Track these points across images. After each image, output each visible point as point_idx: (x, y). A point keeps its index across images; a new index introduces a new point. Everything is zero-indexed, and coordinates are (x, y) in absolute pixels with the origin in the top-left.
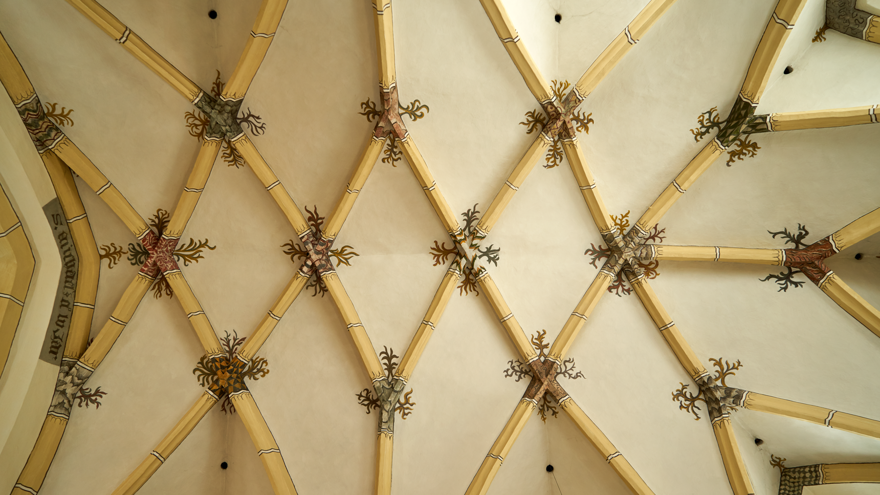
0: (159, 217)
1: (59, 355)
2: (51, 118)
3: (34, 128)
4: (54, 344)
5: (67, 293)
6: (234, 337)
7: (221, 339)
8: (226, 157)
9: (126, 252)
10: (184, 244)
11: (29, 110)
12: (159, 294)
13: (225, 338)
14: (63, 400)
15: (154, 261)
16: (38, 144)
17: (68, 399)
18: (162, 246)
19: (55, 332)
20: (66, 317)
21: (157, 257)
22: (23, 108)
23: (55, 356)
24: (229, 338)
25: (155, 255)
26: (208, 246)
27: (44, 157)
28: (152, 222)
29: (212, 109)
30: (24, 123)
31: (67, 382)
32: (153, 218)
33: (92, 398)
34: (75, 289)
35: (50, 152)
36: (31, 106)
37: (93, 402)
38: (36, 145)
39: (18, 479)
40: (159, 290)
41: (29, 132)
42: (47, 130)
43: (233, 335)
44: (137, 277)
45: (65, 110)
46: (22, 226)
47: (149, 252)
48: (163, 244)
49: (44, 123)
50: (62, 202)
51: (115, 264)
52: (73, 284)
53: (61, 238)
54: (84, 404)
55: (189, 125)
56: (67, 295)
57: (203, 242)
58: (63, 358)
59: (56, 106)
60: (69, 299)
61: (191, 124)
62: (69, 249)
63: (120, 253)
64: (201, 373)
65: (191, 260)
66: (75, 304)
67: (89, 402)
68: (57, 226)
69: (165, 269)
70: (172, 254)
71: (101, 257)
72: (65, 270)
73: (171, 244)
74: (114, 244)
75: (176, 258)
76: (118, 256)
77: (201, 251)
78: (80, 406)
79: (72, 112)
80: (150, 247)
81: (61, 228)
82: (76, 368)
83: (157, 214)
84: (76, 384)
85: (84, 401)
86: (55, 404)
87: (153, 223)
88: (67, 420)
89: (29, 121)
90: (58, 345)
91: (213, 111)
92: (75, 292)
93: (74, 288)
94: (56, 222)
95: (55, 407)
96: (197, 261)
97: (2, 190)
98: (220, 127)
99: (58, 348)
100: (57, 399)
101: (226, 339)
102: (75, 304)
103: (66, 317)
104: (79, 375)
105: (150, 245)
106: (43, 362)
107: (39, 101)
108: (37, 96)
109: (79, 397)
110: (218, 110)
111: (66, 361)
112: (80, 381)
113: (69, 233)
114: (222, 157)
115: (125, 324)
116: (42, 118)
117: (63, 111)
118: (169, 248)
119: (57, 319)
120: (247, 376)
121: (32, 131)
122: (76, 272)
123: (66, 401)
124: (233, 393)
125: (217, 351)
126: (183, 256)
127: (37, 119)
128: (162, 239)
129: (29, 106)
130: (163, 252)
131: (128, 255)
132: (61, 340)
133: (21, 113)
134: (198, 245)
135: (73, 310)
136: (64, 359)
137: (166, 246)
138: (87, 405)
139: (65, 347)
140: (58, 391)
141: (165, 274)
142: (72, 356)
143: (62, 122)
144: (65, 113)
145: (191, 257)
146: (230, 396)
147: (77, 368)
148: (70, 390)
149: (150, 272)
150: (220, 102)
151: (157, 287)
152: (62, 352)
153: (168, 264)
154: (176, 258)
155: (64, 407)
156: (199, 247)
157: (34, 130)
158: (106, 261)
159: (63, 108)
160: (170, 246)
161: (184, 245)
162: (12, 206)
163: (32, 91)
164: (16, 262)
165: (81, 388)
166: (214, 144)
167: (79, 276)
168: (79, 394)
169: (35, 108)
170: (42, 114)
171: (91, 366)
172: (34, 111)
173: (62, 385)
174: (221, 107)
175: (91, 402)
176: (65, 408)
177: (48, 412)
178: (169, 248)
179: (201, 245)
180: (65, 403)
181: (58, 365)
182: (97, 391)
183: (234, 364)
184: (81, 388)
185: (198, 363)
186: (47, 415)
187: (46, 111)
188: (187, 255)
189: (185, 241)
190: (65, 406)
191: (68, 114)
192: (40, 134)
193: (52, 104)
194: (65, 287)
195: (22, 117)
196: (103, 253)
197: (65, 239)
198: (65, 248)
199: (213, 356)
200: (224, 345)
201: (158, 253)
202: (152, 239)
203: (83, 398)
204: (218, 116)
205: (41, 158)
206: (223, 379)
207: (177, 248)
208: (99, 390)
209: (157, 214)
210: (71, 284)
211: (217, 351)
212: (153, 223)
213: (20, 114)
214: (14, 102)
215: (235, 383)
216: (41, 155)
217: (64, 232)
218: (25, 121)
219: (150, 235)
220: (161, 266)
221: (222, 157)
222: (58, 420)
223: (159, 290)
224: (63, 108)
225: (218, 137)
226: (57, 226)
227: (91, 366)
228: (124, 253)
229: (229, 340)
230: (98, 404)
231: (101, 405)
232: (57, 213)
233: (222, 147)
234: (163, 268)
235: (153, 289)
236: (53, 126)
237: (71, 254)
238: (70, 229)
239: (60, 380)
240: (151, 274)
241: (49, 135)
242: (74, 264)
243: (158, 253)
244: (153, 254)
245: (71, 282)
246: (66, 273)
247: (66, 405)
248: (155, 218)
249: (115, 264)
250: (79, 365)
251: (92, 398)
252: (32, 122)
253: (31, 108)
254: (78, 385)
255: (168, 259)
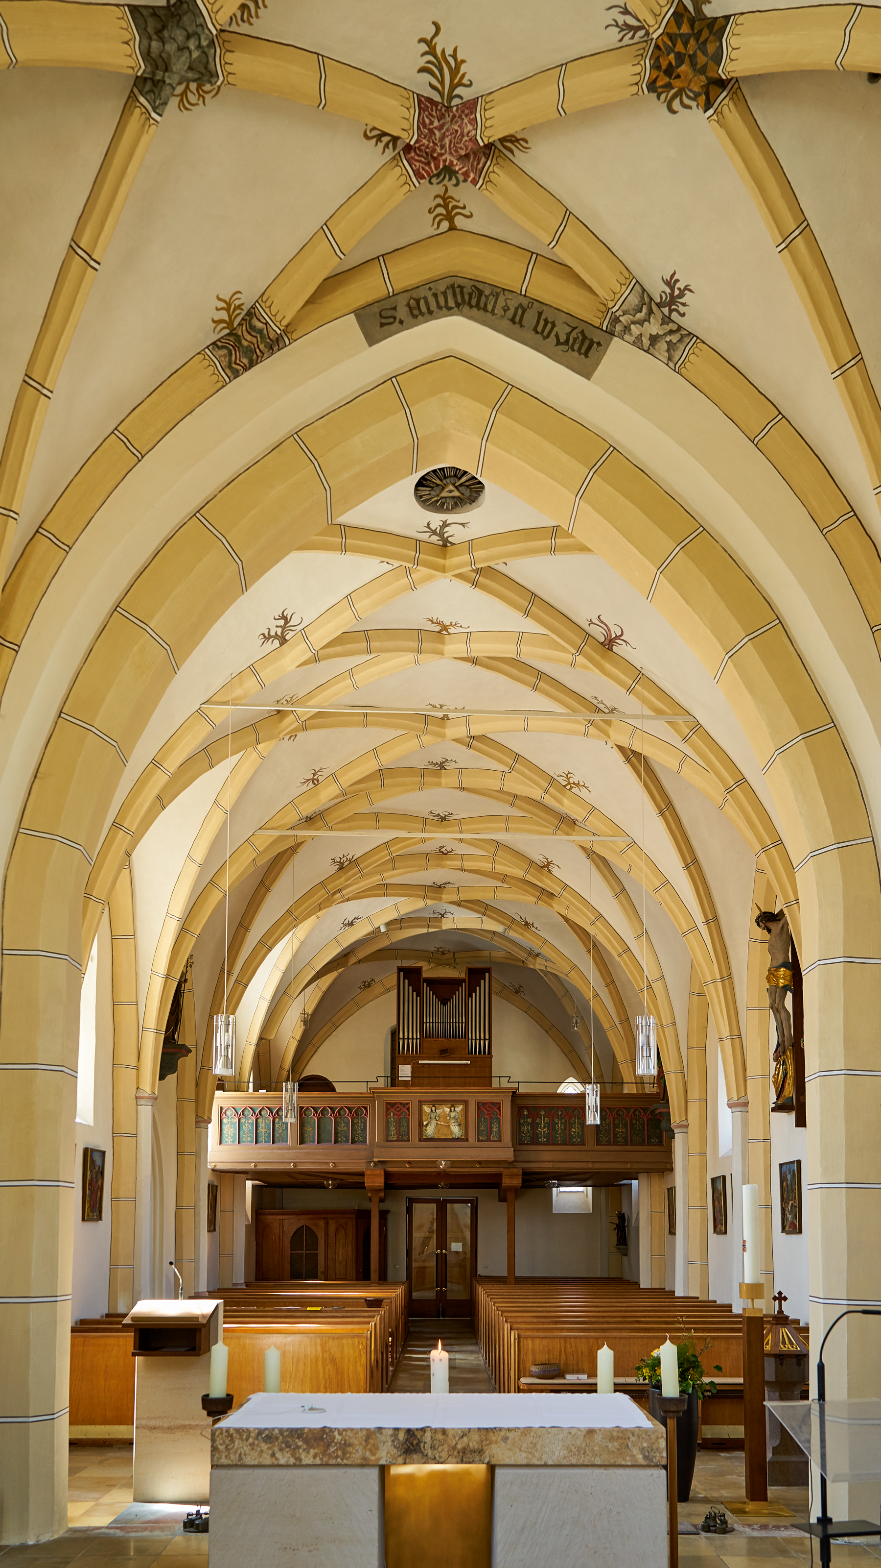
0: (379, 135)
1: (596, 336)
2: (236, 323)
3: (255, 356)
4: (576, 347)
5: (503, 308)
6: (621, 12)
7: (621, 40)
8: (250, 15)
9: (444, 188)
10: (430, 84)
11: (230, 362)
12: (521, 142)
13: (619, 32)
14: (666, 342)
15: (458, 160)
16: (277, 347)
17: (665, 335)
18: (431, 144)
19: (558, 343)
20: (540, 314)
21: (451, 153)
22: (227, 371)
23: (595, 345)
24: (621, 23)
25: (448, 157)
26: (433, 38)
27: (294, 336)
28: (388, 148)
29: (164, 82)
30: (250, 369)
31: (638, 333)
32: (381, 145)
33: (675, 294)
34: (499, 290)
35: (288, 330)
36: (223, 359)
37: (682, 295)
38: (279, 350)
39: (749, 438)
40: (514, 141)
41: (261, 362)
42: (254, 334)
43: (615, 13)
44: (485, 192)
45: (219, 307)
46: (398, 375)
47: (441, 167)
48: (427, 143)
49: (244, 339)
50: (362, 305)
51: (464, 208)
52: (492, 294)
53: (416, 312)
54: (682, 309)
55: (201, 99)
56: (506, 309)
57: (424, 47)
58: (602, 329)
59: (216, 319)
60: (512, 305)
61: (199, 95)
62: (435, 295)
63: (445, 199)
64: (678, 99)
65: (461, 72)
66: (523, 293)
67: (681, 300)
68: (398, 320)
69: (474, 143)
70: (449, 108)
71: (452, 228)
72: (466, 308)
73: (427, 121)
74: (431, 209)
75: (456, 101)
76: (450, 202)
77: (443, 51)
78: (683, 315)
79: (221, 297)
80: (432, 165)
81: (402, 312)
82: (620, 316)
83: (374, 140)
84: (647, 317)
85: (678, 306)
86: (667, 359)
87: (391, 145)
88: (698, 341)
89: (246, 363)
90: (581, 338)
91: (168, 81)
92: (504, 289)
93: (498, 291)
94: (392, 320)
95: (671, 361)
96: (463, 61)
97: (347, 405)
98: (194, 61)
99: (585, 337)
100: (660, 354)
101: (622, 30)
102: (523, 293)
103: (540, 314)
104: (634, 309)
105: (428, 164)
106: (597, 374)
107: (214, 343)
108: (207, 347)
109: (671, 311)
110: (164, 74)
111: (607, 326)
112: (644, 310)
113: (410, 293)
114: (251, 24)
115: (568, 213)
116: (238, 339)
117: (222, 309)
118: (436, 123)
119: (539, 336)
120: (703, 6)
121: (260, 359)
122: (473, 283)
123: (668, 339)
124: (720, 71)
125: (638, 69)
126: (453, 87)
127: (241, 349)
128: (417, 145)
129: (225, 363)
130: (442, 139)
131: (450, 184)
132: (574, 328)
133: (236, 374)
134: (430, 58)
135: (532, 299)
136: (604, 329)
137: (431, 132)
138: (684, 305)
139: (586, 322)
140: (649, 348)
141: (482, 144)
142: (603, 312)
143: (239, 307)
144: (224, 305)
145: (454, 72)
146: (724, 77)
147: (622, 314)
148: (654, 327)
149: (478, 164)
150: (148, 73)
151: (509, 145)
152: (594, 328)
153: (466, 131)
154: (456, 101)
155: (675, 344)
156: (435, 56)
157: (258, 356)
158: (459, 221)
159: (217, 309)
160: (431, 123)
161: (430, 85)
162: (368, 391)
163: (201, 357)
164: (447, 394)
165: (657, 304)
166: (229, 57)
167: (480, 280)
168: (666, 310)
169: (225, 351)
170: (232, 338)
171: (624, 288)
172: (230, 355)
173: (642, 341)
174: (157, 69)
175: (681, 298)
176: (678, 341)
177: (675, 371)
178: (436, 123)
179: (432, 51)
180: (671, 340)
181: (612, 339)
182: (668, 283)
183: (666, 49)
184: (657, 304)
185: (659, 98)
186: (678, 373)
187: (227, 331)
188: (452, 80)
189: (423, 84)
190: (674, 341)
191: (225, 301)
192: (262, 347)
193: (214, 325)
194: (493, 312)
195: (242, 373)
196: (445, 225)
197: (418, 301)
198: (433, 306)
199: (644, 86)
200: (633, 37)
201: (443, 151)
202: (419, 156)
203: (673, 307)
204: (174, 70)
205: (296, 340)
206: (690, 81)
207: (437, 98)
208: (667, 280)
209: (374, 140)
210: (491, 297)
211: (638, 69)
212: (391, 145)
213: (238, 376)
214: (223, 387)
215: (705, 53)
216: (291, 341)
217: (408, 305)
218: (246, 369)
219: (412, 158)
220: (467, 149)
221: (251, 24)
222: (692, 358)
223: (514, 141)
224: (217, 309)
225: (213, 51)
226: (398, 320)
227: (624, 288)
228: (446, 190)
229: (625, 24)
230: (687, 288)
231: (689, 286)
232: (378, 316)
233: (231, 29)
234: (470, 145)
235: (511, 151)
236: (242, 324)
237: (442, 293)
238: (403, 290)
239: (634, 341)
240: (483, 160)
241: (260, 332)
242: (459, 286)
243: (443, 151)
244: (445, 161)
245: (487, 297)
246: (471, 307)
247: (675, 338)
248: (381, 141)
249: (464, 208)
250: (618, 310)
251: (675, 294)
252: (246, 357)
253: (227, 360)
254: (650, 312)
255: (456, 128)
